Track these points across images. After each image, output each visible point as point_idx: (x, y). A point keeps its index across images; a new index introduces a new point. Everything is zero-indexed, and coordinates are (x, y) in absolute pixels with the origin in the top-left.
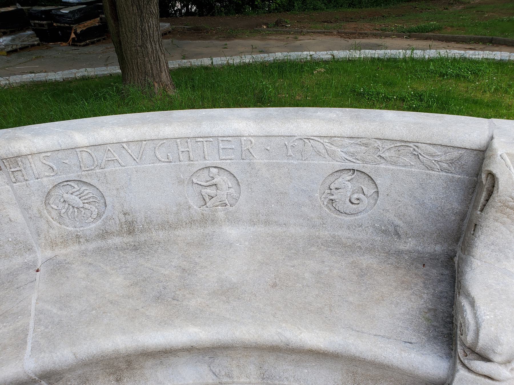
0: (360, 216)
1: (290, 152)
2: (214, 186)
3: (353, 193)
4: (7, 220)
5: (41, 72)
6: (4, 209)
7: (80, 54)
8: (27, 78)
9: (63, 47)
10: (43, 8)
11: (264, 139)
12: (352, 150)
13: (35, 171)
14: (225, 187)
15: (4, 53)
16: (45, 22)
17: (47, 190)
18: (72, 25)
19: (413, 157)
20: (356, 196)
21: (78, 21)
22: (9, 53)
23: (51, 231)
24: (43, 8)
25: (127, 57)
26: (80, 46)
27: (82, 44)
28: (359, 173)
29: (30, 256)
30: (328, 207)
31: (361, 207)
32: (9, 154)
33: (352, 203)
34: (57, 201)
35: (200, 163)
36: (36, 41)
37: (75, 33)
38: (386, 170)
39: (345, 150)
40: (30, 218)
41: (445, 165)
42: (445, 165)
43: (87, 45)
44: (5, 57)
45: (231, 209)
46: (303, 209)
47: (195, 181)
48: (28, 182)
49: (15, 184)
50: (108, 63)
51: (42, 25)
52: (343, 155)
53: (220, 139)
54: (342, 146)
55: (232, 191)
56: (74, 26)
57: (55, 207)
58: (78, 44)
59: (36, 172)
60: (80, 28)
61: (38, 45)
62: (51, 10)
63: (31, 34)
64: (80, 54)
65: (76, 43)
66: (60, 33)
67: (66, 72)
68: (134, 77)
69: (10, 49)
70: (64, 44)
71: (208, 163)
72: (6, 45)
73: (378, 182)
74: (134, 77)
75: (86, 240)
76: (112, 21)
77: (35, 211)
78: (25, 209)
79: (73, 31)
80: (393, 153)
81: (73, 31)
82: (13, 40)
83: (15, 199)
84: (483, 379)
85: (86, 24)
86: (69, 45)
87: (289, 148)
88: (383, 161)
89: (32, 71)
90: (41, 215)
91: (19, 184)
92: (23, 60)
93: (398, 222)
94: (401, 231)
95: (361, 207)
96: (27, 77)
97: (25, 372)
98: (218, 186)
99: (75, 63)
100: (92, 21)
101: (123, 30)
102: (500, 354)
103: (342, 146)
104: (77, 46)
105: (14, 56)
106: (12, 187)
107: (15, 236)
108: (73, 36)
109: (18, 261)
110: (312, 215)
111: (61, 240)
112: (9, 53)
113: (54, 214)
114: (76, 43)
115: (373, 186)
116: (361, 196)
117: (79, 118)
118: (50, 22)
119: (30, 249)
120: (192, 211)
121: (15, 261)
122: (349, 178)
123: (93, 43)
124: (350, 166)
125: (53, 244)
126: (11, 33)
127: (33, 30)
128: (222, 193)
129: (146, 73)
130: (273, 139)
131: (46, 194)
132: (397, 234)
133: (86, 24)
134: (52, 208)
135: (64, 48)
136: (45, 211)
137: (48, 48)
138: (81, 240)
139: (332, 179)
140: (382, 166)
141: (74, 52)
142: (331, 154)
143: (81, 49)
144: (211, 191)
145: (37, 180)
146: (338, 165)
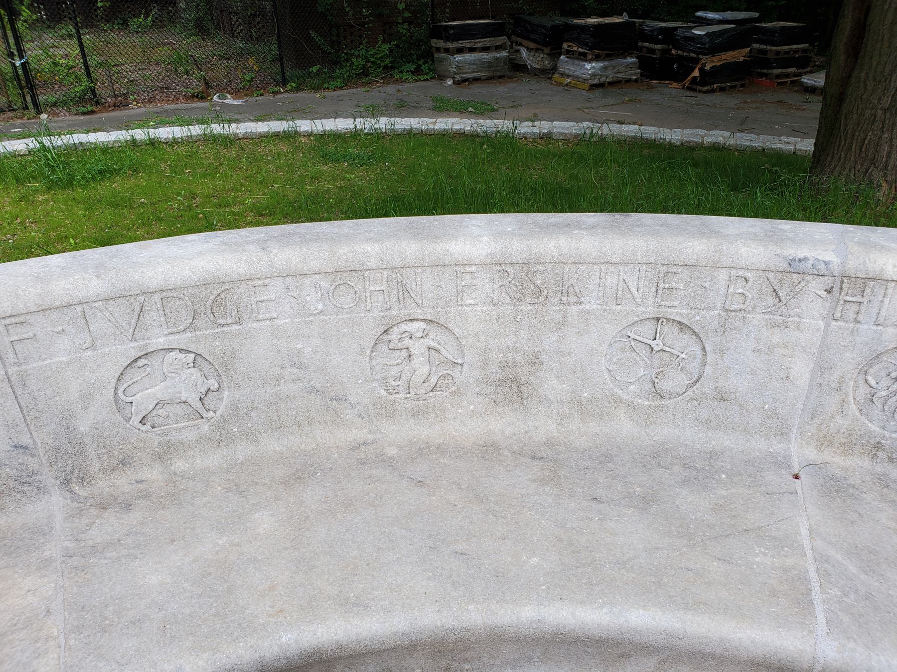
4: (783, 374)
5: (634, 124)
6: (792, 356)
7: (698, 105)
8: (628, 131)
9: (672, 89)
10: (664, 25)
13: (884, 310)
15: (587, 86)
16: (658, 47)
17: (880, 349)
18: (701, 56)
21: (714, 50)
22: (593, 87)
23: (839, 419)
24: (664, 25)
25: (846, 125)
26: (700, 91)
27: (706, 88)
29: (780, 446)
32: (861, 270)
34: (883, 374)
36: (635, 74)
37: (702, 70)
40: (820, 385)
43: (712, 91)
44: (584, 93)
48: (858, 326)
49: (834, 323)
50: (744, 127)
51: (652, 51)
56: (704, 58)
57: (872, 382)
58: (699, 88)
59: (883, 313)
60: (710, 63)
61: (636, 81)
62: (676, 29)
63: (632, 63)
64: (698, 105)
65: (695, 87)
66: (675, 66)
67: (688, 132)
68: (844, 163)
69: (596, 81)
70: (675, 85)
72: (593, 75)
74: (844, 163)
75: (889, 458)
76: (842, 57)
77: (836, 377)
78: (822, 366)
79: (699, 66)
81: (699, 66)
82: (605, 68)
83: (818, 346)
85: (724, 57)
86: (683, 88)
89: (622, 119)
90: (840, 387)
91: (842, 324)
92: (610, 101)
96: (630, 130)
97: (814, 658)
99: (686, 119)
100: (736, 52)
101: (863, 75)
104: (695, 90)
105: (598, 93)
106: (827, 325)
107: (777, 404)
108: (696, 73)
109: (759, 445)
111: (843, 440)
112: (593, 87)
113: (863, 391)
114: (695, 87)
117: (673, 213)
118: (666, 47)
119: (783, 434)
121: (754, 444)
123: (722, 90)
125: (825, 441)
126: (608, 57)
127: (637, 57)
129: (873, 162)
131: (875, 355)
133: (724, 57)
134: (866, 381)
135: (674, 92)
136: (852, 383)
137: (650, 88)
138: (880, 454)
141: (689, 100)
143: (701, 96)
145: (875, 328)
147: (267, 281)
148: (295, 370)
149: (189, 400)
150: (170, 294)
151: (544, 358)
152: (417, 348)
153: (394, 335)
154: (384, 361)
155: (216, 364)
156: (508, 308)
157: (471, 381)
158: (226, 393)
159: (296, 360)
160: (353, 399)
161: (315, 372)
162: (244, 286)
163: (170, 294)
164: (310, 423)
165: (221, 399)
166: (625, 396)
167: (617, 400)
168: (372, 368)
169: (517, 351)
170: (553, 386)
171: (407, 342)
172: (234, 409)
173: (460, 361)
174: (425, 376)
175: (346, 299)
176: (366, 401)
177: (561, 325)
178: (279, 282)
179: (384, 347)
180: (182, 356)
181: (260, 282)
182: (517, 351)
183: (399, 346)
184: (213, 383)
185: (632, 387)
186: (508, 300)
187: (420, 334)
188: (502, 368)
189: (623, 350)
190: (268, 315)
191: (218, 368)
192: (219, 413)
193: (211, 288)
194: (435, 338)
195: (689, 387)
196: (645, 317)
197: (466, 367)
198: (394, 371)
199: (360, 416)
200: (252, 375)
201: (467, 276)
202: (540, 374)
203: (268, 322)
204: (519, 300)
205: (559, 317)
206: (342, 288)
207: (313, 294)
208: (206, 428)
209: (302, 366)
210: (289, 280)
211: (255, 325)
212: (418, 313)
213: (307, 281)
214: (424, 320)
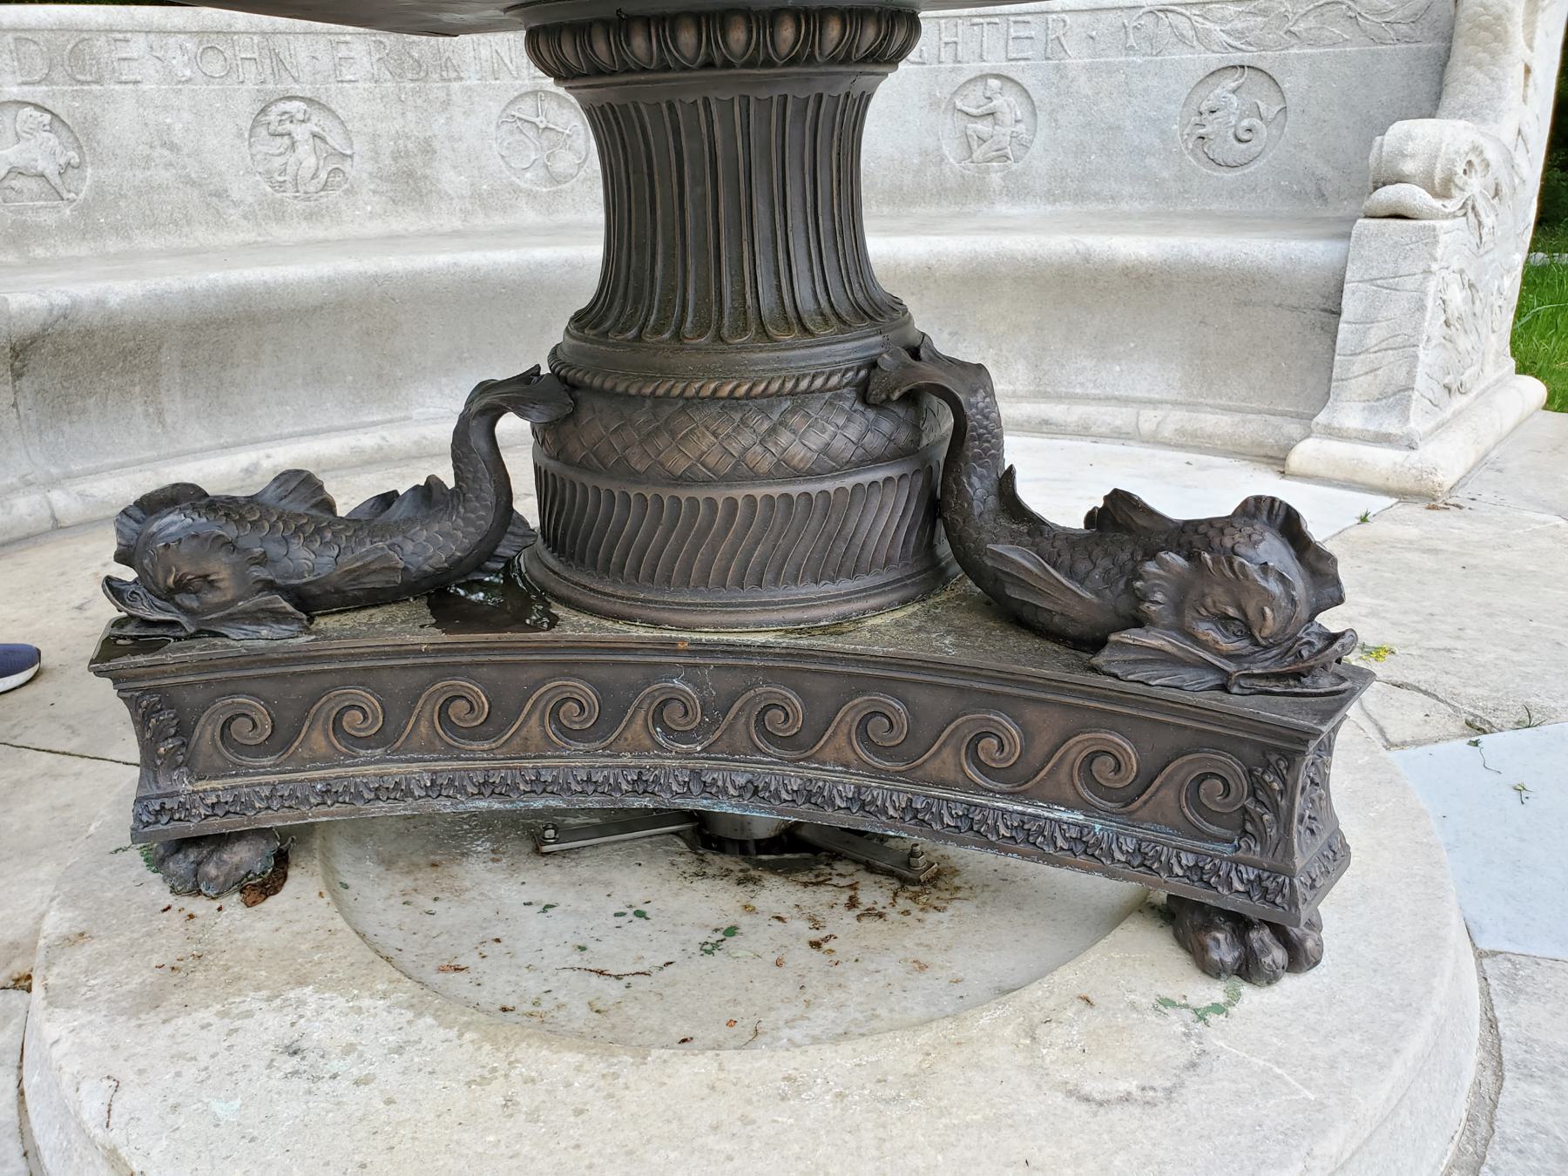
0: (1252, 168)
1: (1131, 41)
2: (990, 118)
3: (1241, 118)
11: (1086, 17)
12: (1239, 25)
14: (1009, 119)
19: (1347, 24)
20: (1245, 123)
28: (1253, 72)
30: (1195, 156)
31: (1254, 147)
33: (1240, 141)
35: (972, 68)
38: (1299, 57)
39: (1228, 27)
41: (1404, 28)
42: (1404, 28)
45: (1015, 167)
46: (1150, 161)
47: (959, 105)
52: (1225, 37)
53: (1012, 18)
54: (1223, 20)
55: (1021, 127)
71: (987, 67)
73: (1285, 86)
80: (1312, 22)
84: (1391, 221)
87: (1130, 31)
88: (1294, 41)
93: (1323, 169)
94: (1328, 189)
95: (1254, 147)
98: (999, 115)
102: (1413, 156)
103: (1223, 20)
110: (1165, 174)
115: (1276, 97)
116: (1256, 122)
120: (947, 170)
122: (1234, 85)
124: (1236, 58)
128: (1003, 130)
130: (1103, 15)
132: (1322, 196)
139: (1202, 92)
140: (1293, 51)
142: (1203, 38)
144: (983, 127)
146: (1215, 60)
147: (129, 35)
148: (166, 152)
149: (47, 172)
150: (23, 35)
151: (436, 144)
152: (301, 132)
153: (273, 116)
154: (265, 149)
155: (76, 130)
156: (390, 86)
157: (365, 176)
158: (89, 171)
159: (165, 137)
160: (235, 196)
161: (189, 156)
162: (103, 38)
163: (23, 35)
164: (189, 223)
165: (84, 179)
166: (523, 185)
167: (517, 190)
168: (252, 156)
169: (408, 138)
170: (451, 179)
171: (288, 126)
172: (99, 189)
173: (349, 152)
174: (312, 170)
175: (215, 67)
176: (250, 199)
177: (447, 104)
178: (141, 38)
179: (262, 132)
180: (37, 114)
181: (120, 36)
182: (408, 138)
183: (280, 129)
184: (74, 157)
185: (528, 175)
186: (389, 76)
187: (300, 116)
188: (395, 159)
189: (511, 133)
190: (132, 78)
191: (77, 133)
192: (82, 196)
193: (68, 35)
194: (318, 122)
195: (580, 166)
196: (523, 90)
197: (356, 158)
198: (277, 162)
199: (245, 217)
200: (118, 151)
201: (343, 47)
202: (436, 164)
203: (131, 86)
204: (400, 76)
205: (442, 95)
206: (210, 53)
207: (179, 57)
208: (68, 212)
209: (173, 147)
210: (152, 36)
211: (117, 87)
212: (296, 89)
213: (172, 40)
214: (302, 99)
